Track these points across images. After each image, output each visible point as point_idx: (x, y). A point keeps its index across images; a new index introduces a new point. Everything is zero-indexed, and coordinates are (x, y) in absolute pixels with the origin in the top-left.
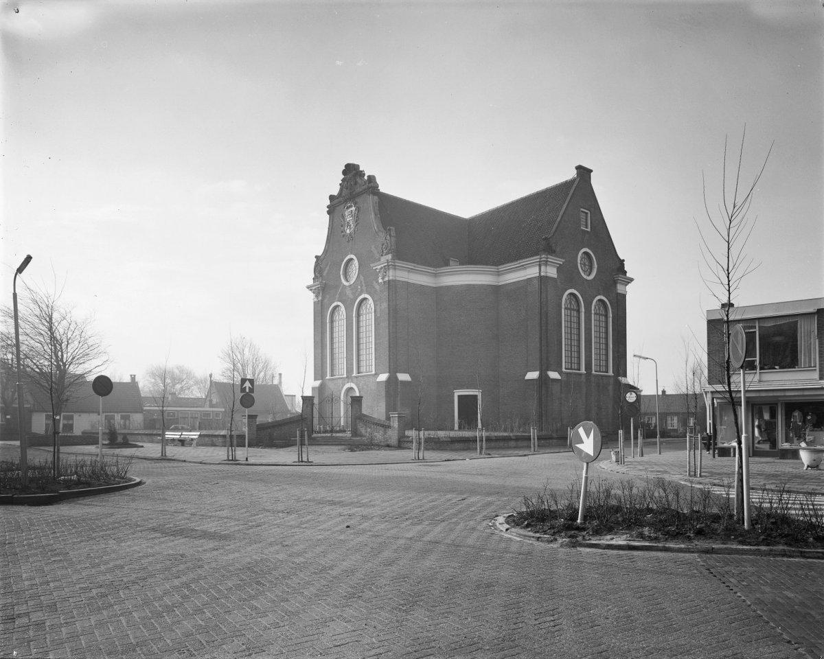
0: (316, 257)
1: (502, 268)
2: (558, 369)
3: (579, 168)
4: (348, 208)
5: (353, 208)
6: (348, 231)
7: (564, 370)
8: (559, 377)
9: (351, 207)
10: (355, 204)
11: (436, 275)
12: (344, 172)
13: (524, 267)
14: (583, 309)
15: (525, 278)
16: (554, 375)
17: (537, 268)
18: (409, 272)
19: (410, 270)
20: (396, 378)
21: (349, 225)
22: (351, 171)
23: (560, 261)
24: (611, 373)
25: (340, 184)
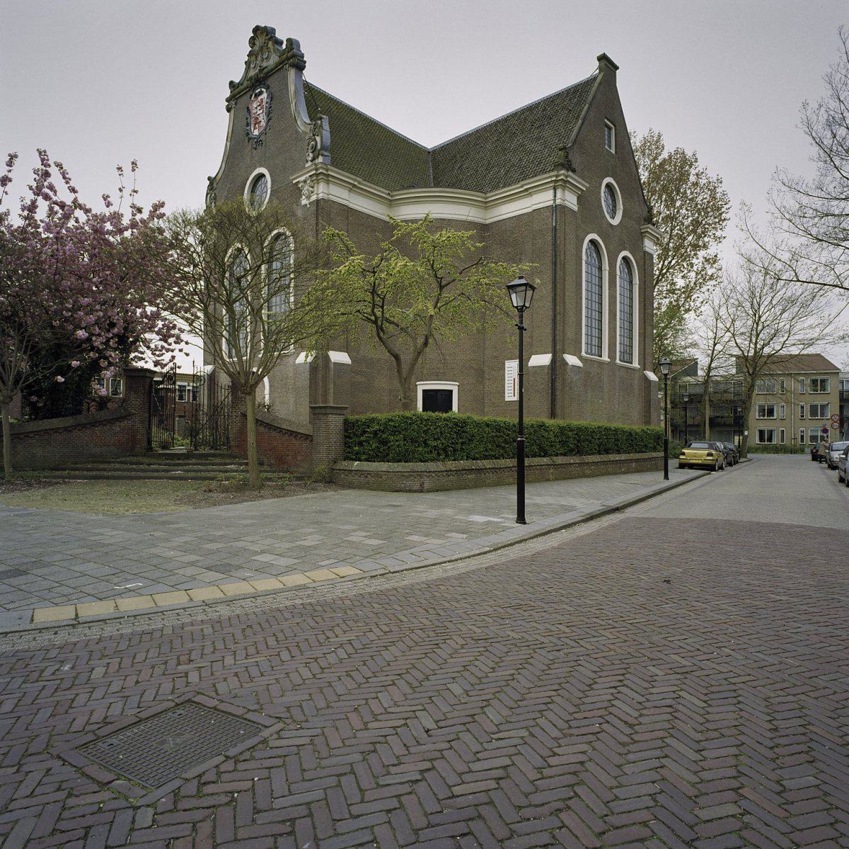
0: (209, 179)
1: (493, 195)
2: (577, 353)
3: (603, 58)
4: (257, 96)
5: (265, 95)
6: (256, 132)
7: (583, 354)
8: (579, 364)
9: (261, 93)
10: (267, 88)
11: (391, 203)
12: (252, 42)
13: (528, 193)
14: (606, 266)
15: (530, 210)
16: (572, 360)
17: (551, 192)
18: (350, 190)
19: (353, 188)
20: (327, 358)
21: (257, 122)
22: (263, 36)
23: (584, 186)
24: (636, 364)
25: (246, 62)
